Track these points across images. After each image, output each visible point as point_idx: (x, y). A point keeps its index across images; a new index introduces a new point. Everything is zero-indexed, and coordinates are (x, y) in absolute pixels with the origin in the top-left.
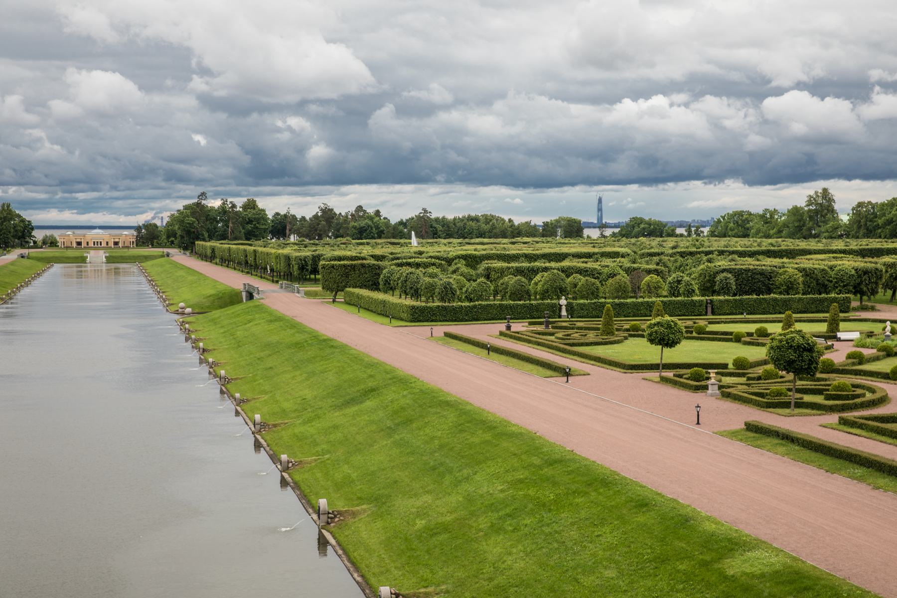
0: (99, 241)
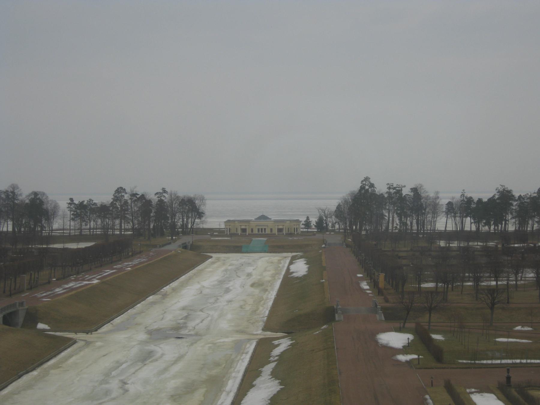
0: (263, 227)
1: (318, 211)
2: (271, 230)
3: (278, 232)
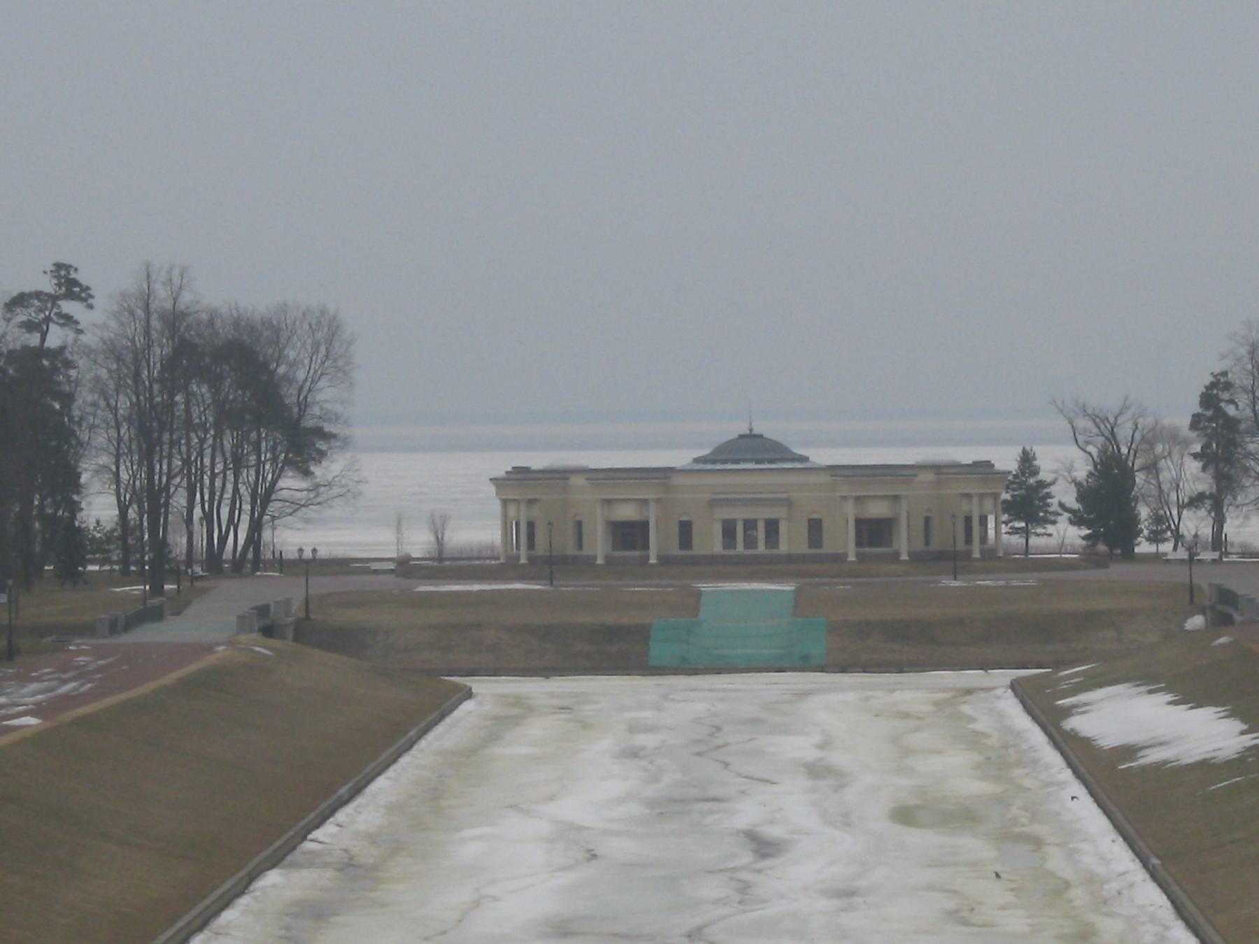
0: (762, 514)
1: (1071, 423)
2: (815, 527)
3: (859, 543)
